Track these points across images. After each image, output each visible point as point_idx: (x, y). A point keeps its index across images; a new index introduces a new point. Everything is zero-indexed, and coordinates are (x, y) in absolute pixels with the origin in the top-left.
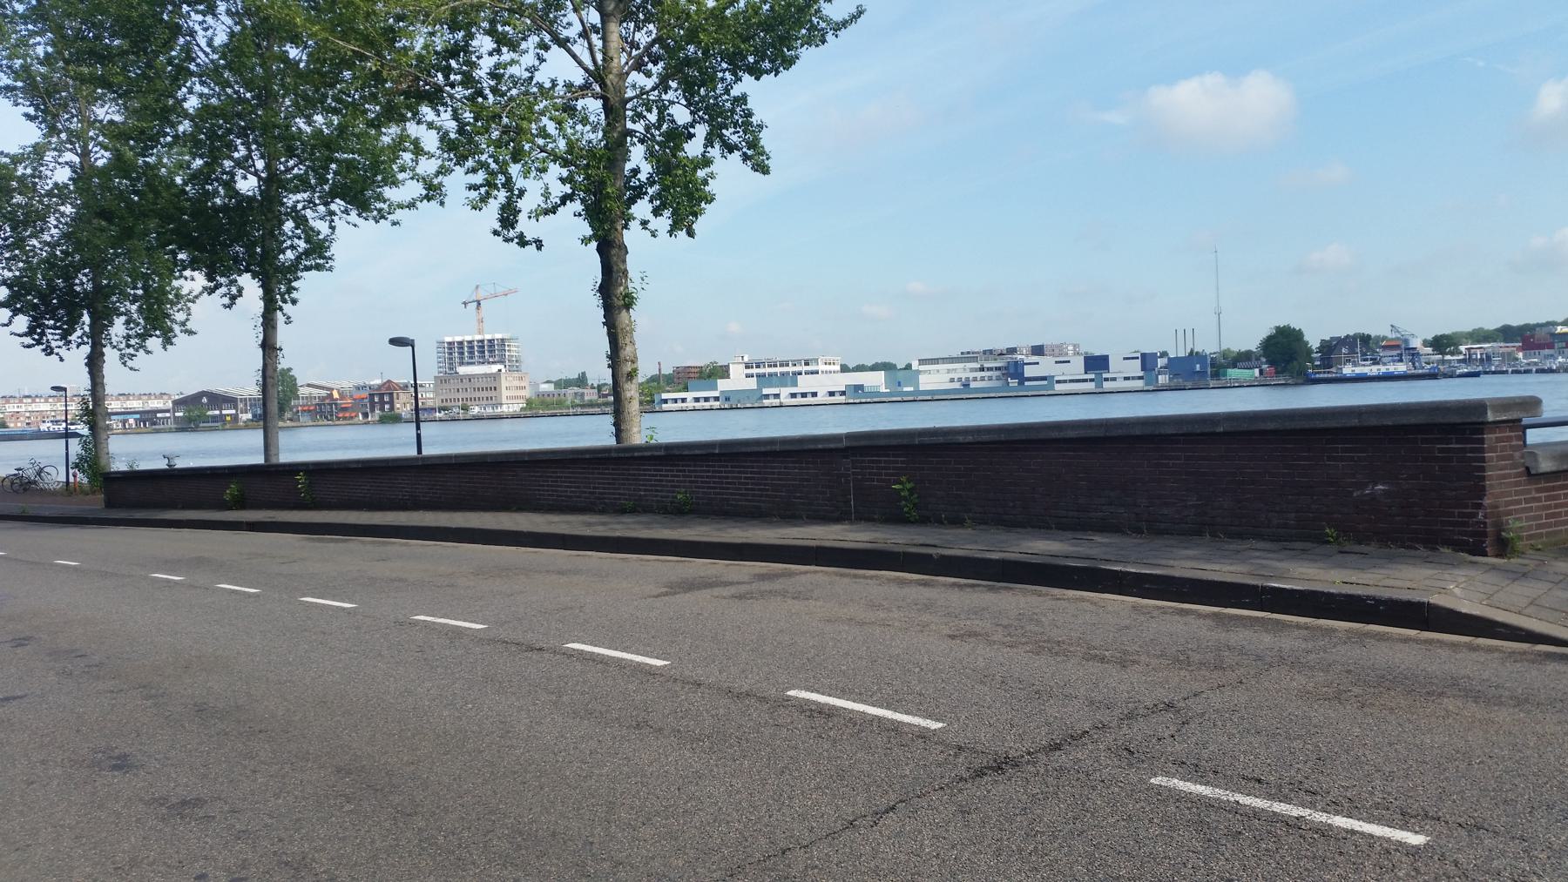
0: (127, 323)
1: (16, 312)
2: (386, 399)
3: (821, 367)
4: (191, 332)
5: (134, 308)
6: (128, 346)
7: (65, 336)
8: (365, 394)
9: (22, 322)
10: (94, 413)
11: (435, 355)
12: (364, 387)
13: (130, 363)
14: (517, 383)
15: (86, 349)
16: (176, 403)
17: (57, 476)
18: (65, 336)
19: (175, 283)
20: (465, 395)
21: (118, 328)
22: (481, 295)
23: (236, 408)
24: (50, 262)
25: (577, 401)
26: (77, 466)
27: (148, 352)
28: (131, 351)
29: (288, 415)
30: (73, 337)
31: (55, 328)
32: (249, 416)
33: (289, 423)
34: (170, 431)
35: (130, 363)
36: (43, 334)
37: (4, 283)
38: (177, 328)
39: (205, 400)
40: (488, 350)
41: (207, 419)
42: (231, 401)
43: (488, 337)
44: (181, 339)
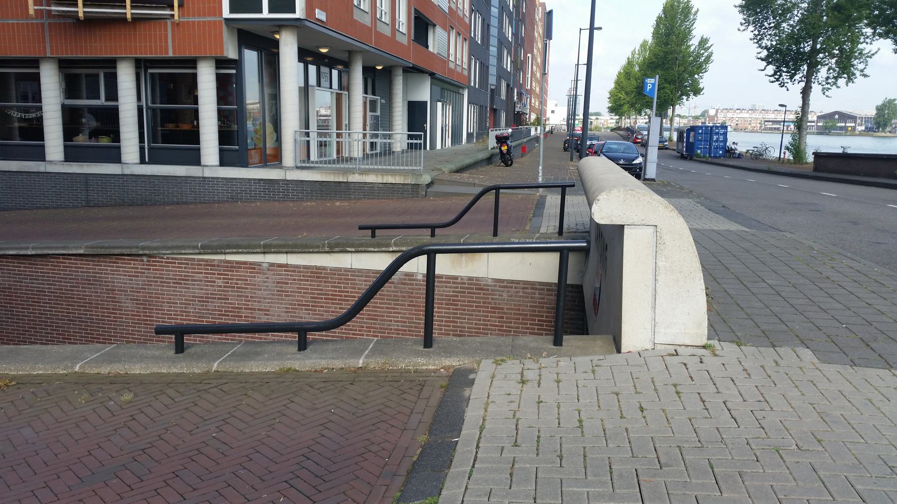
0: (829, 69)
1: (769, 63)
3: (598, 286)
4: (865, 76)
5: (834, 61)
6: (828, 83)
7: (791, 78)
9: (771, 69)
10: (800, 123)
13: (827, 93)
15: (803, 84)
16: (819, 117)
17: (775, 154)
18: (791, 78)
19: (860, 46)
21: (823, 72)
23: (855, 122)
24: (791, 36)
26: (787, 148)
27: (838, 87)
28: (829, 86)
29: (888, 129)
30: (797, 77)
31: (787, 72)
32: (863, 128)
33: (888, 134)
35: (827, 93)
36: (781, 76)
38: (858, 73)
39: (837, 117)
41: (836, 128)
42: (853, 118)
44: (859, 79)
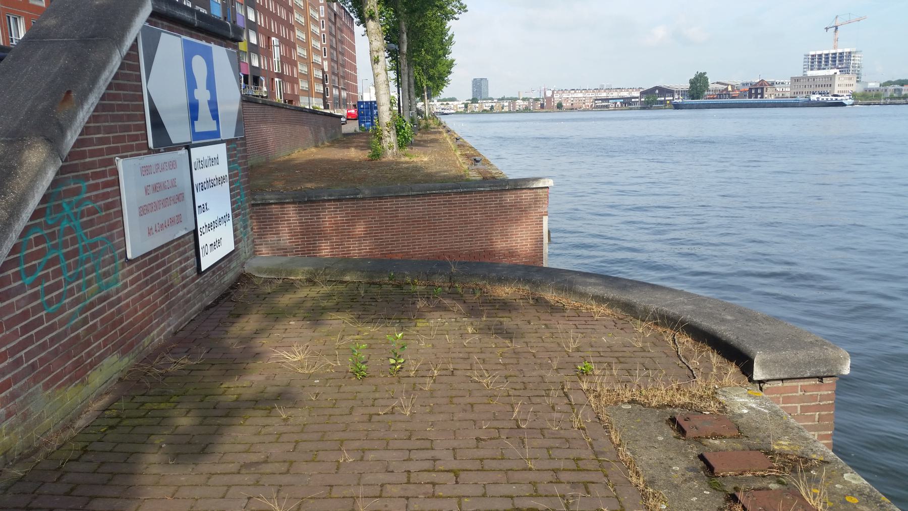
2: (759, 91)
8: (747, 88)
11: (803, 64)
12: (747, 84)
14: (847, 82)
16: (641, 93)
20: (807, 90)
22: (838, 22)
25: (895, 95)
34: (637, 109)
37: (2, 142)
39: (657, 91)
40: (840, 61)
42: (671, 92)
43: (840, 51)
